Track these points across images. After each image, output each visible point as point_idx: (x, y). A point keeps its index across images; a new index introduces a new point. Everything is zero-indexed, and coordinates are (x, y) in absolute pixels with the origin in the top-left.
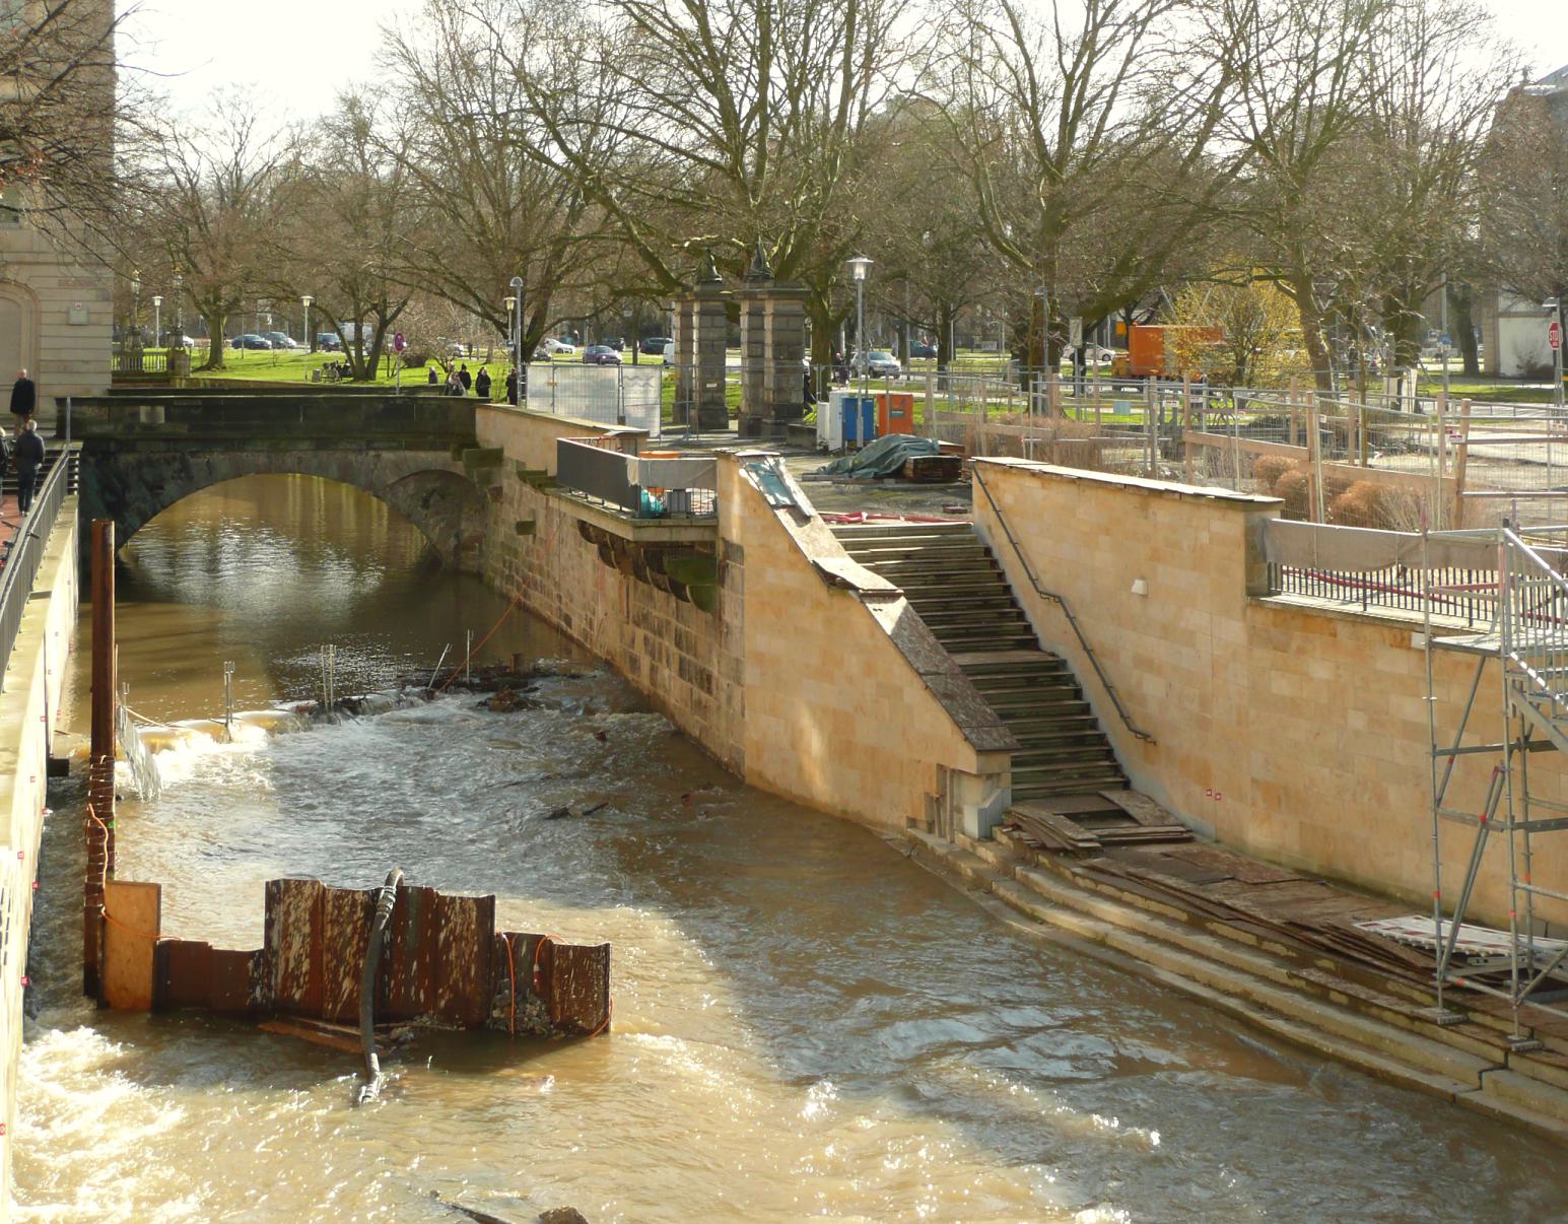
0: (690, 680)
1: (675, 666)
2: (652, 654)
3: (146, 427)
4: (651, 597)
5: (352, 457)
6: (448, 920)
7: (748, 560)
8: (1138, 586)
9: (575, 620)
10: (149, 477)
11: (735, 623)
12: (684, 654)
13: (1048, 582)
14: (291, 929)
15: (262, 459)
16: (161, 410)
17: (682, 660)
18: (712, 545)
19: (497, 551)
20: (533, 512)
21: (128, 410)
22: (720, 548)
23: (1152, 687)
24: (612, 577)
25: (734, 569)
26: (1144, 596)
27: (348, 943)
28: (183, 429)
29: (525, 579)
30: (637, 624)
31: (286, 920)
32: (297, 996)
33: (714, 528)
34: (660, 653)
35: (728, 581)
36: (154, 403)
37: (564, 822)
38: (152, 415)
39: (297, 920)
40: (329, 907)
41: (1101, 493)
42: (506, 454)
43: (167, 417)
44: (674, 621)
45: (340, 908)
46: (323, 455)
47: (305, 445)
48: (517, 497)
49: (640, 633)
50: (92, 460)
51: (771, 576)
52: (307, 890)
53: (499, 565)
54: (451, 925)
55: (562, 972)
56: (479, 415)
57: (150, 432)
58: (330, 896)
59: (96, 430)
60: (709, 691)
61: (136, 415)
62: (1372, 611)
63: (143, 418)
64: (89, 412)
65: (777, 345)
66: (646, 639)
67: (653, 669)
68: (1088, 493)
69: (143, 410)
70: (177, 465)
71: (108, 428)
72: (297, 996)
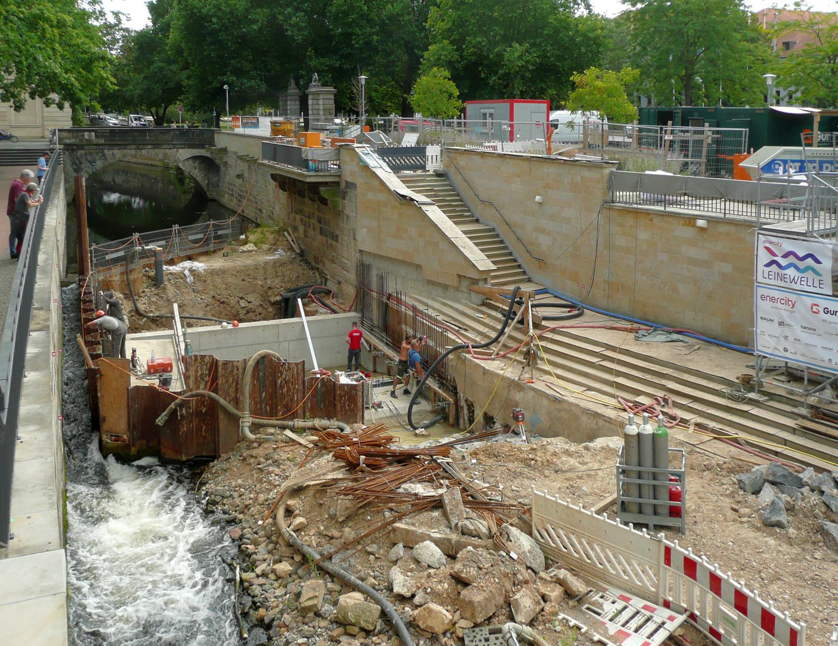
0: (326, 236)
1: (318, 230)
2: (305, 226)
3: (87, 140)
4: (304, 203)
5: (167, 150)
6: (281, 373)
7: (359, 190)
8: (538, 198)
9: (264, 211)
10: (90, 159)
11: (353, 214)
12: (323, 226)
13: (484, 196)
14: (199, 378)
15: (133, 152)
16: (93, 134)
17: (321, 228)
18: (338, 183)
19: (226, 185)
20: (242, 171)
21: (80, 134)
22: (343, 185)
23: (544, 241)
24: (283, 196)
25: (351, 194)
26: (540, 204)
27: (230, 387)
28: (102, 141)
29: (240, 196)
30: (297, 213)
31: (196, 375)
32: (204, 411)
33: (340, 176)
34: (309, 225)
35: (348, 197)
36: (90, 131)
37: (734, 513)
38: (89, 136)
39: (202, 374)
40: (220, 369)
41: (516, 161)
42: (228, 149)
43: (96, 136)
44: (316, 212)
45: (226, 369)
46: (157, 150)
47: (150, 147)
48: (234, 164)
49: (298, 217)
50: (67, 152)
51: (370, 196)
52: (207, 359)
53: (227, 190)
54: (284, 376)
55: (341, 397)
56: (216, 136)
57: (89, 143)
58: (220, 364)
59: (68, 141)
60: (337, 241)
61: (83, 136)
62: (668, 209)
63: (86, 137)
64: (65, 134)
65: (324, 110)
66: (301, 219)
67: (305, 231)
68: (508, 160)
69: (86, 134)
70: (100, 154)
71: (73, 141)
72: (204, 411)
